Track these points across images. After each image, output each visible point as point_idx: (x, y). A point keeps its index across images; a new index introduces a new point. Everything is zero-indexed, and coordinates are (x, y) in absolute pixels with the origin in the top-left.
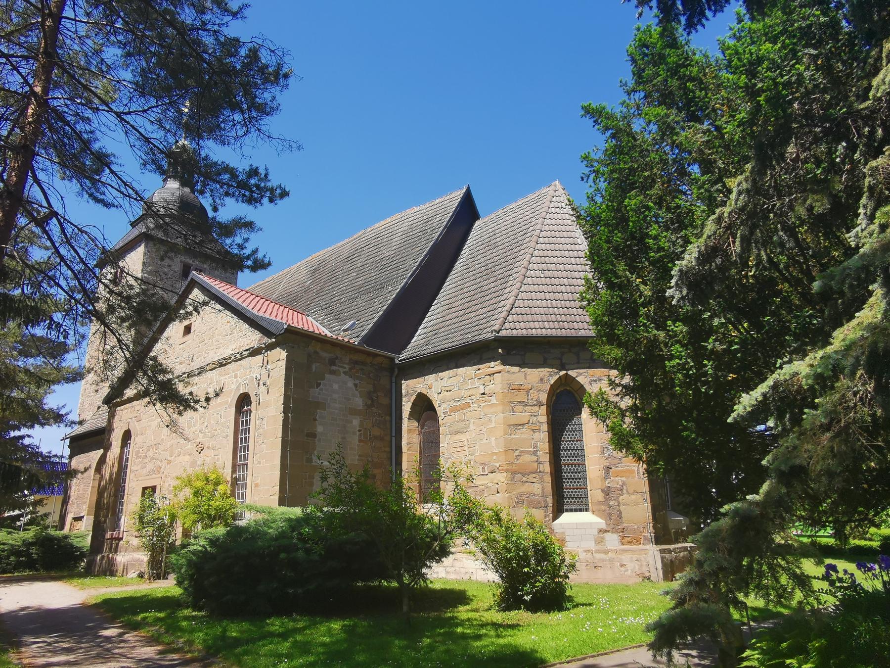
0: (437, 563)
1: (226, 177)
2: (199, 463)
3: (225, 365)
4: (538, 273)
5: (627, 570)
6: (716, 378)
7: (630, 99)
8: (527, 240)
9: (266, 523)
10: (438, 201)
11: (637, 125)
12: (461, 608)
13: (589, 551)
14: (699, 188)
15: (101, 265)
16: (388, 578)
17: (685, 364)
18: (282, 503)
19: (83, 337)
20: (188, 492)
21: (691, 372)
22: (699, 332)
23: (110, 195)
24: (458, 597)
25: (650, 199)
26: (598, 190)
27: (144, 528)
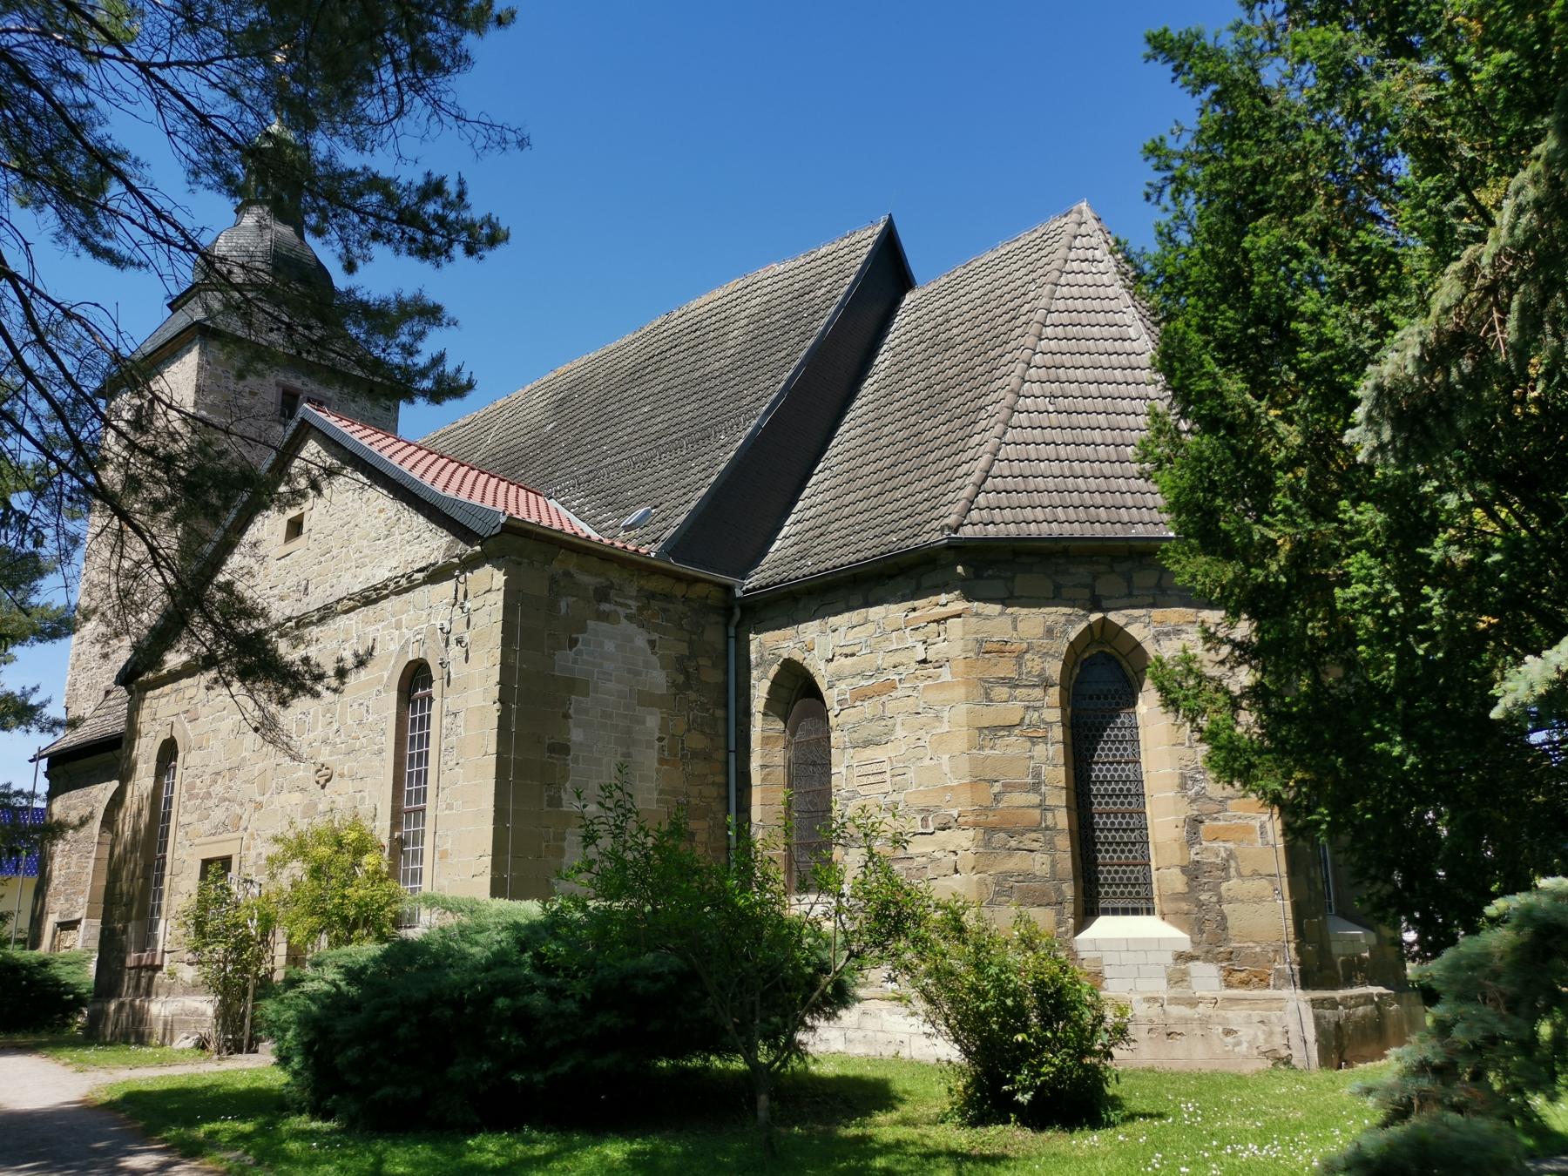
0: (828, 1019)
1: (375, 198)
2: (321, 807)
3: (375, 601)
4: (1042, 403)
5: (1238, 1044)
6: (1451, 624)
7: (1251, 18)
8: (1018, 331)
9: (463, 933)
10: (823, 251)
11: (1271, 74)
12: (880, 1117)
13: (1155, 1000)
14: (1416, 207)
15: (109, 390)
16: (725, 1050)
17: (1378, 595)
18: (497, 890)
19: (75, 541)
20: (298, 868)
21: (1392, 612)
22: (1411, 524)
23: (126, 238)
24: (868, 1095)
25: (1303, 233)
26: (1183, 216)
27: (207, 945)
